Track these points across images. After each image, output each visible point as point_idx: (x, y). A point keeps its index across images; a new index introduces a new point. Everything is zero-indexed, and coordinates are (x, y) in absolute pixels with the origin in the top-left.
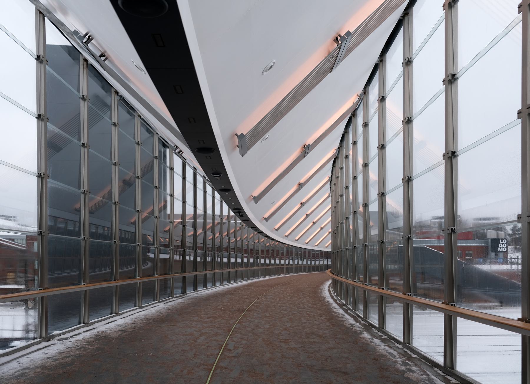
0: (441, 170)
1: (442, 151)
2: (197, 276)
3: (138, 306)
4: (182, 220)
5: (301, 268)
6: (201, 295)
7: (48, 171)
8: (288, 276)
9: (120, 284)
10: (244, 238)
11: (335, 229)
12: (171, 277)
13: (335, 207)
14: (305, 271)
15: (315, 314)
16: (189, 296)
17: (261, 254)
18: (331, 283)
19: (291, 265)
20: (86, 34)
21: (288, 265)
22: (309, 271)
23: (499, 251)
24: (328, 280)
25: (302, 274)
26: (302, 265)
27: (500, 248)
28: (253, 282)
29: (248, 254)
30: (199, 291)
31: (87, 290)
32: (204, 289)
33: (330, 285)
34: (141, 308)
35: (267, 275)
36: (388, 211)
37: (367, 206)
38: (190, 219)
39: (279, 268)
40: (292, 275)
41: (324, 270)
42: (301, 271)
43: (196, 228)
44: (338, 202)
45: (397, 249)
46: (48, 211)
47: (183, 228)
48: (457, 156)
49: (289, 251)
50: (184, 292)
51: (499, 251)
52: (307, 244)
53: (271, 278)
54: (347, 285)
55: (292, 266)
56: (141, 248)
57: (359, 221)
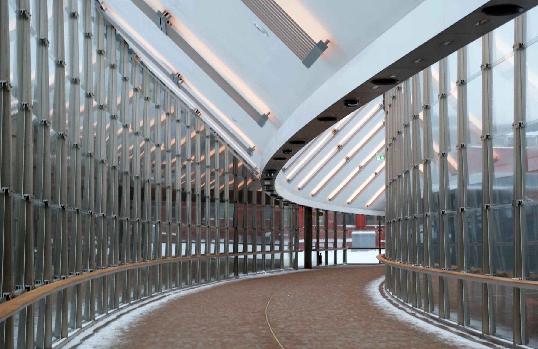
7: (33, 146)
11: (390, 183)
12: (138, 267)
13: (390, 144)
15: (362, 307)
20: (178, 73)
24: (378, 276)
28: (224, 284)
31: (93, 279)
32: (167, 290)
33: (382, 284)
44: (394, 139)
50: (236, 275)
54: (426, 275)
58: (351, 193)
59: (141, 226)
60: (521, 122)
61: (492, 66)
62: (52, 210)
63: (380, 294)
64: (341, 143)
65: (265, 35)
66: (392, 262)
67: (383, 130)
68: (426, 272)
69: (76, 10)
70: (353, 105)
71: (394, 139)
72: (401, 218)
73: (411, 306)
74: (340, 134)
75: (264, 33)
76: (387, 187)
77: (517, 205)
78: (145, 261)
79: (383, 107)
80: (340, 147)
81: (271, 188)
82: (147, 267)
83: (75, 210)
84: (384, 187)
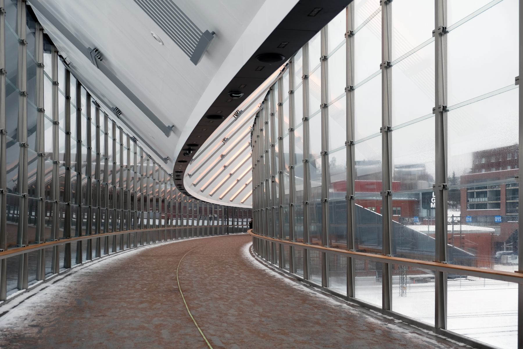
0: (380, 138)
1: (379, 125)
2: (117, 236)
3: (23, 289)
4: (65, 162)
5: (190, 230)
6: (91, 269)
8: (181, 242)
9: (29, 251)
10: (131, 187)
13: (256, 165)
14: (201, 234)
16: (76, 272)
17: (161, 211)
18: (252, 245)
19: (163, 226)
21: (176, 227)
22: (206, 234)
23: (431, 207)
24: (248, 242)
25: (198, 238)
26: (186, 226)
27: (433, 203)
29: (142, 211)
30: (84, 264)
31: (4, 259)
33: (251, 247)
34: (28, 291)
35: (190, 236)
36: (457, 176)
37: (308, 162)
38: (139, 163)
39: (164, 230)
40: (185, 239)
41: (223, 233)
42: (196, 235)
43: (81, 171)
45: (315, 208)
46: (416, 169)
47: (66, 171)
48: (392, 131)
49: (203, 209)
51: (431, 207)
52: (221, 200)
53: (167, 243)
55: (175, 228)
56: (27, 201)
57: (295, 177)
58: (232, 195)
59: (131, 214)
60: (352, 141)
61: (328, 105)
62: (60, 205)
63: (249, 252)
64: (226, 164)
65: (161, 43)
66: (257, 235)
67: (251, 159)
68: (281, 243)
69: (42, 62)
70: (237, 95)
71: (258, 161)
72: (260, 210)
73: (265, 260)
74: (226, 158)
75: (160, 42)
76: (254, 190)
77: (324, 202)
78: (19, 246)
79: (251, 144)
80: (225, 167)
81: (181, 187)
82: (54, 247)
83: (54, 201)
84: (251, 192)
